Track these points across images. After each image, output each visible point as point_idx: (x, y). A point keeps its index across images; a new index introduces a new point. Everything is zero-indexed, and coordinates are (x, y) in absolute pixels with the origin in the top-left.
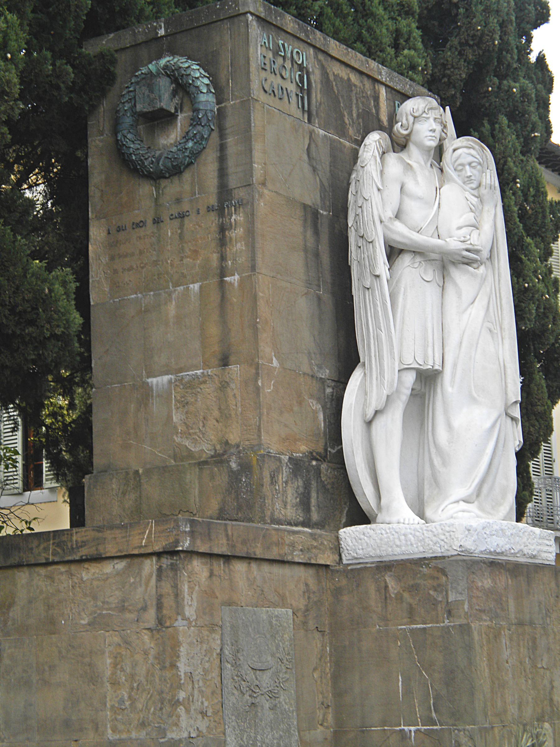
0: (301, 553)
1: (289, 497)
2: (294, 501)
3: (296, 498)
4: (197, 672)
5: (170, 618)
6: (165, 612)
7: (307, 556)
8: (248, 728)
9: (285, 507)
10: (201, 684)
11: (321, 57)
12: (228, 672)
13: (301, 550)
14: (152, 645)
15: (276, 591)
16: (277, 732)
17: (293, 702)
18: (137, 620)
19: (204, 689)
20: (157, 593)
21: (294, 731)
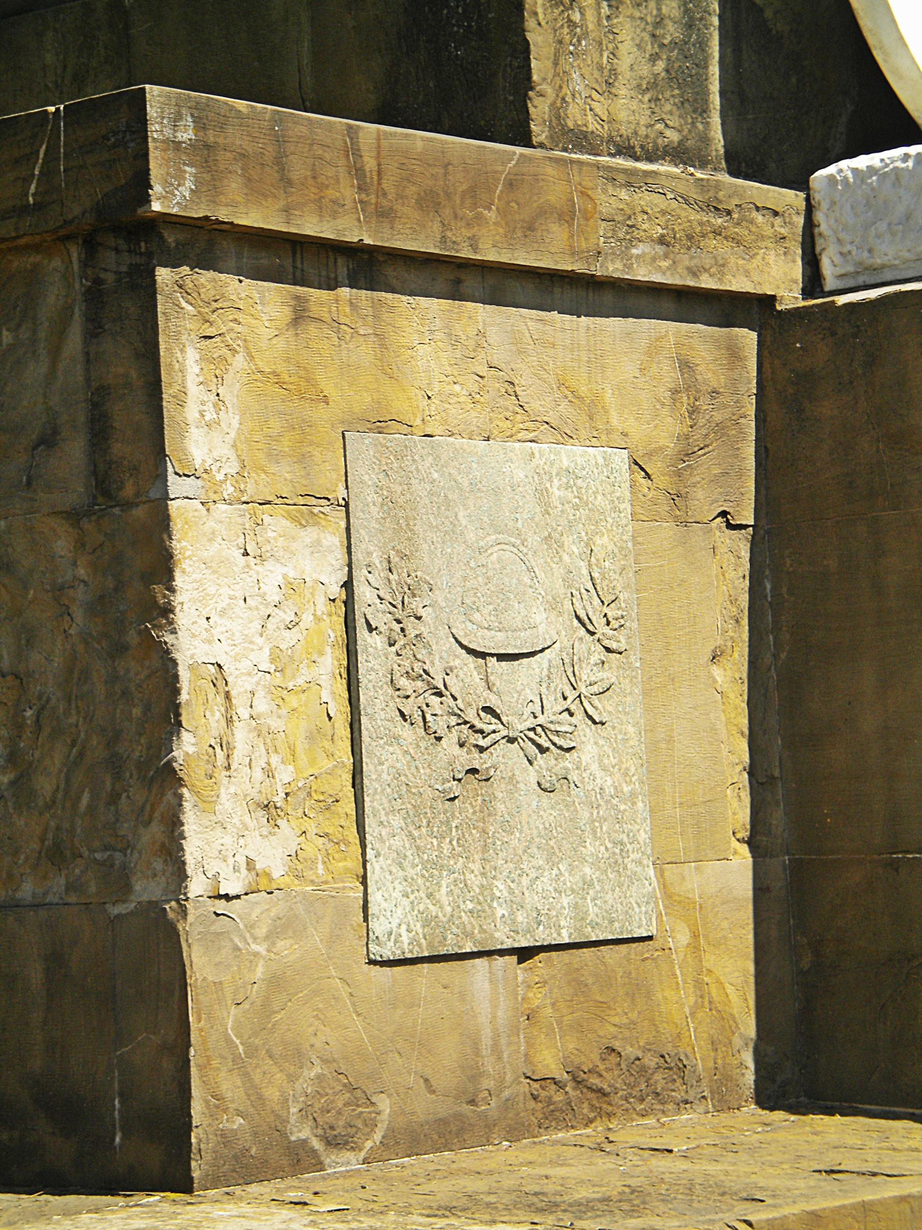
0: (660, 250)
1: (624, 49)
2: (645, 70)
3: (654, 58)
4: (246, 665)
5: (135, 470)
6: (118, 449)
7: (685, 260)
8: (453, 856)
9: (609, 82)
10: (262, 705)
12: (373, 663)
13: (662, 241)
14: (82, 572)
15: (561, 384)
16: (571, 869)
17: (631, 765)
18: (29, 483)
19: (275, 724)
20: (88, 380)
21: (639, 862)
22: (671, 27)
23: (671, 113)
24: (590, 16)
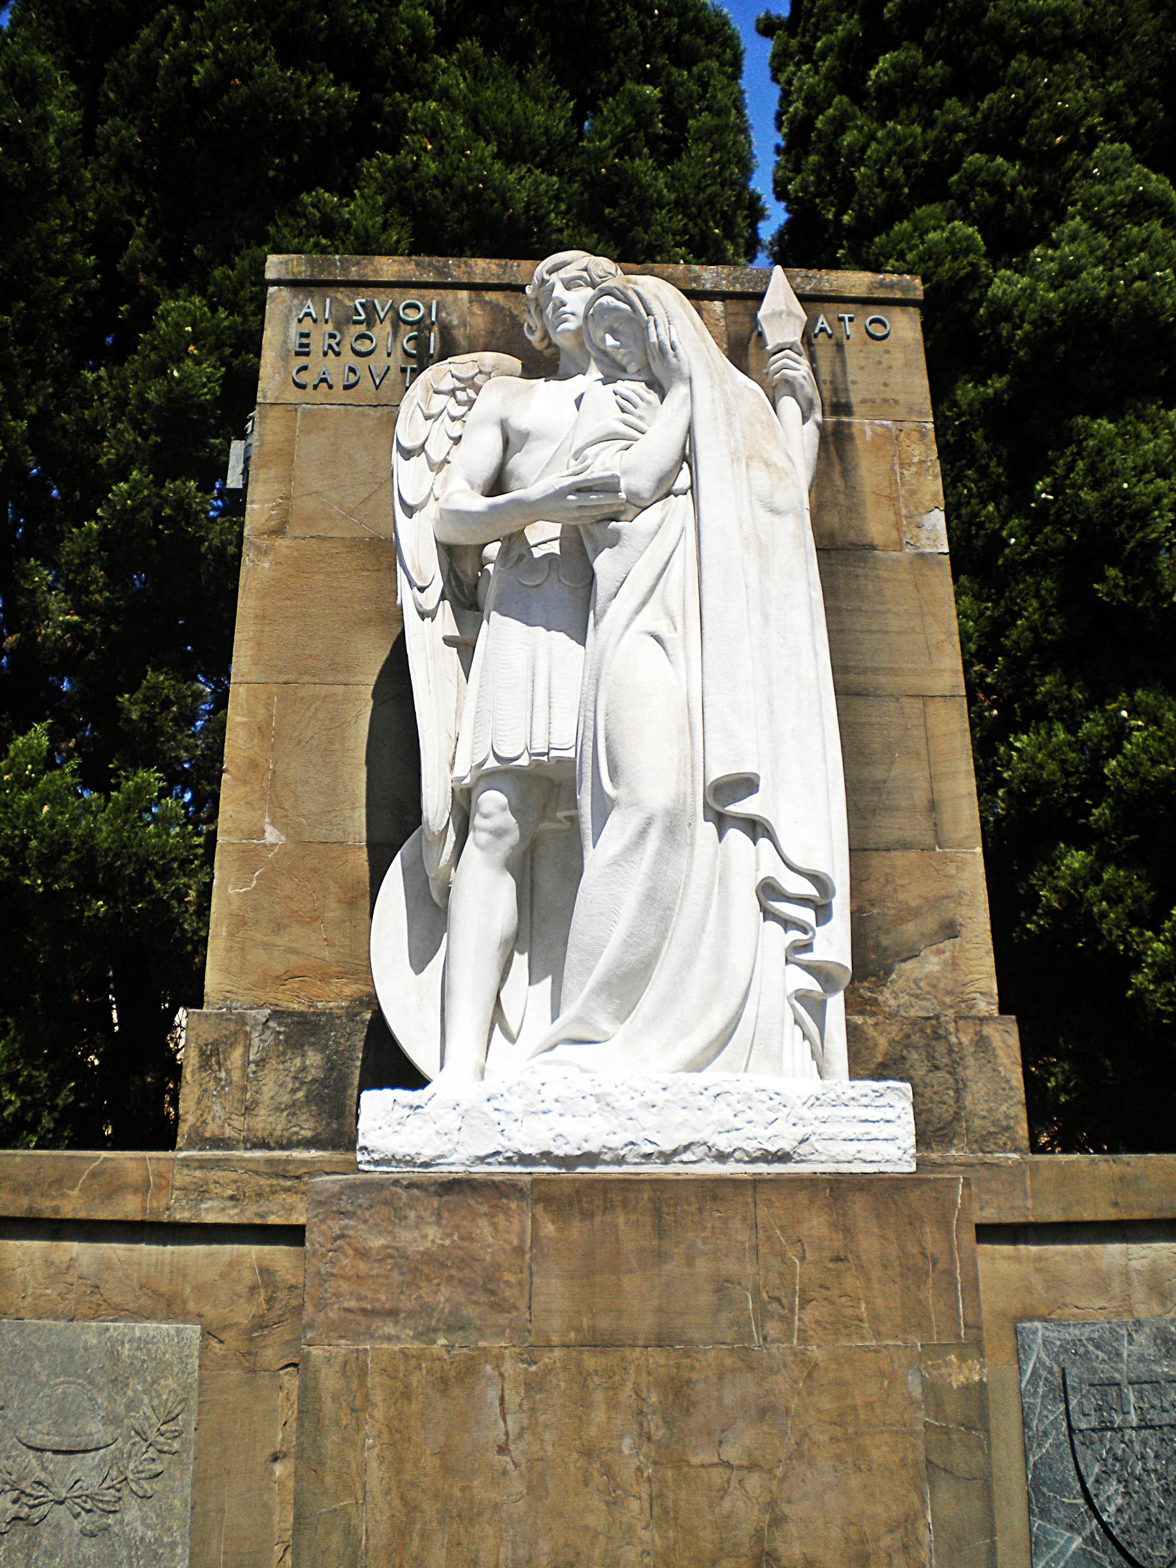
0: (230, 1203)
2: (285, 1098)
3: (294, 1091)
11: (489, 296)
13: (232, 1198)
22: (313, 1071)
24: (236, 1075)
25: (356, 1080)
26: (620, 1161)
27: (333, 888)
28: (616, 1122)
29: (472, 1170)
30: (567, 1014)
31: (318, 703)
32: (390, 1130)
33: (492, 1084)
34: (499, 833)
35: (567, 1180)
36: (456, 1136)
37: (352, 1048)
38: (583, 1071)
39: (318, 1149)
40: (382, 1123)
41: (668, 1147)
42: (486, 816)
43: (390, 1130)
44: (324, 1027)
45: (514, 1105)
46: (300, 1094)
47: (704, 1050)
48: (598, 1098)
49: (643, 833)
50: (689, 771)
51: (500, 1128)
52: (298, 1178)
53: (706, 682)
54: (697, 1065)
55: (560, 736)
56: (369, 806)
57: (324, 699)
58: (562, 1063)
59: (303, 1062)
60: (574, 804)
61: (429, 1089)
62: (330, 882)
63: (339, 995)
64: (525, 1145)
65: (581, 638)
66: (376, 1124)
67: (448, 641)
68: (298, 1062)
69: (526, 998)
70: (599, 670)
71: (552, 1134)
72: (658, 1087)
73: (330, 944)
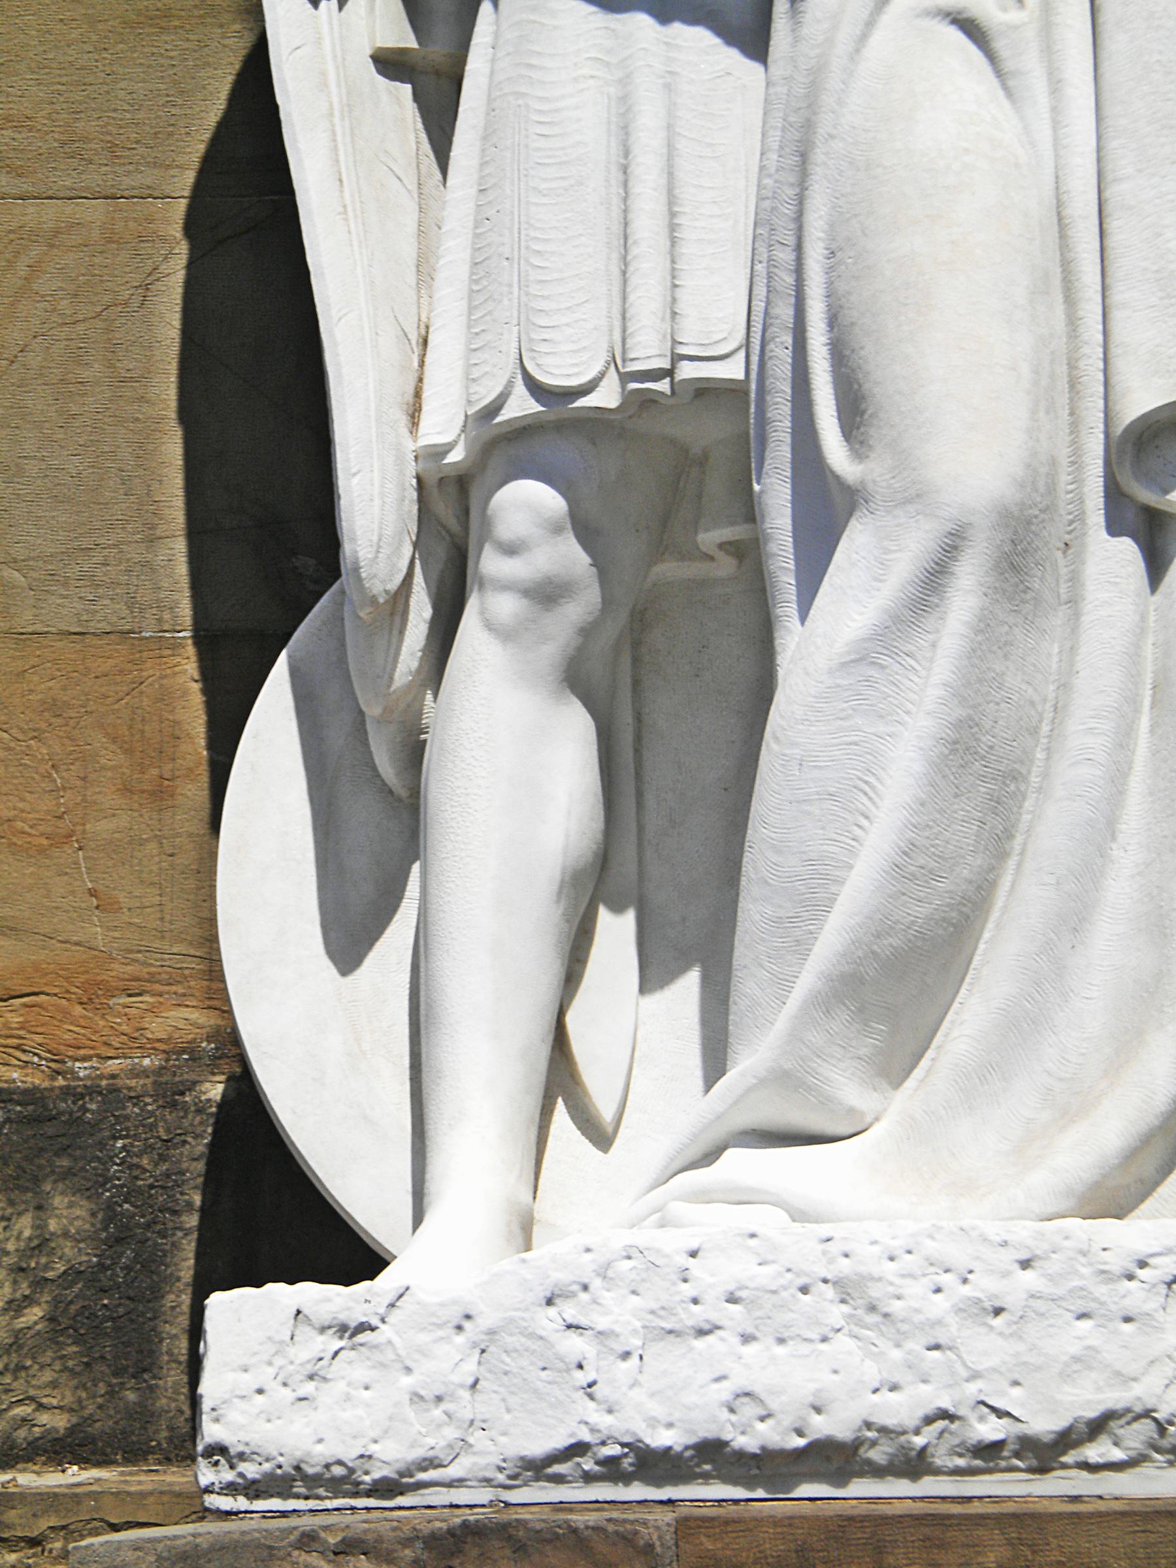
3: (16, 1306)
22: (68, 1249)
23: (54, 1385)
25: (186, 1266)
26: (915, 1465)
27: (110, 756)
28: (896, 1354)
29: (514, 1497)
30: (749, 1061)
31: (35, 252)
32: (288, 1394)
33: (555, 1256)
34: (546, 594)
35: (775, 1521)
36: (465, 1406)
37: (172, 1181)
38: (798, 1215)
39: (84, 1462)
40: (265, 1376)
41: (1043, 1424)
42: (511, 550)
43: (288, 1394)
44: (95, 1126)
45: (618, 1312)
46: (34, 1314)
47: (1131, 1155)
48: (845, 1290)
49: (935, 578)
50: (1063, 400)
51: (582, 1378)
52: (34, 1542)
53: (1113, 145)
54: (1113, 1197)
55: (710, 324)
56: (195, 532)
57: (53, 238)
58: (743, 1198)
59: (40, 1227)
60: (749, 510)
61: (386, 1281)
62: (99, 739)
63: (136, 1041)
64: (653, 1422)
65: (753, 40)
66: (249, 1381)
67: (389, 64)
68: (25, 1225)
69: (634, 1026)
70: (808, 126)
71: (724, 1391)
72: (1007, 1259)
73: (104, 903)
